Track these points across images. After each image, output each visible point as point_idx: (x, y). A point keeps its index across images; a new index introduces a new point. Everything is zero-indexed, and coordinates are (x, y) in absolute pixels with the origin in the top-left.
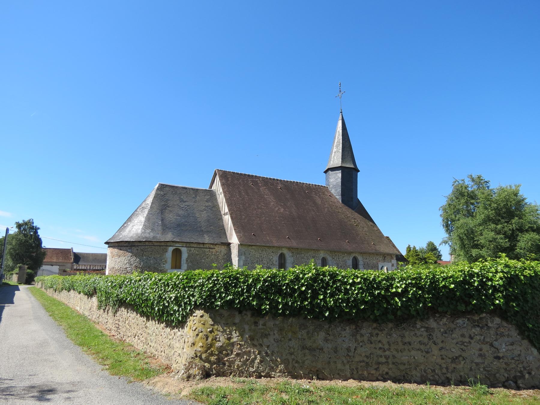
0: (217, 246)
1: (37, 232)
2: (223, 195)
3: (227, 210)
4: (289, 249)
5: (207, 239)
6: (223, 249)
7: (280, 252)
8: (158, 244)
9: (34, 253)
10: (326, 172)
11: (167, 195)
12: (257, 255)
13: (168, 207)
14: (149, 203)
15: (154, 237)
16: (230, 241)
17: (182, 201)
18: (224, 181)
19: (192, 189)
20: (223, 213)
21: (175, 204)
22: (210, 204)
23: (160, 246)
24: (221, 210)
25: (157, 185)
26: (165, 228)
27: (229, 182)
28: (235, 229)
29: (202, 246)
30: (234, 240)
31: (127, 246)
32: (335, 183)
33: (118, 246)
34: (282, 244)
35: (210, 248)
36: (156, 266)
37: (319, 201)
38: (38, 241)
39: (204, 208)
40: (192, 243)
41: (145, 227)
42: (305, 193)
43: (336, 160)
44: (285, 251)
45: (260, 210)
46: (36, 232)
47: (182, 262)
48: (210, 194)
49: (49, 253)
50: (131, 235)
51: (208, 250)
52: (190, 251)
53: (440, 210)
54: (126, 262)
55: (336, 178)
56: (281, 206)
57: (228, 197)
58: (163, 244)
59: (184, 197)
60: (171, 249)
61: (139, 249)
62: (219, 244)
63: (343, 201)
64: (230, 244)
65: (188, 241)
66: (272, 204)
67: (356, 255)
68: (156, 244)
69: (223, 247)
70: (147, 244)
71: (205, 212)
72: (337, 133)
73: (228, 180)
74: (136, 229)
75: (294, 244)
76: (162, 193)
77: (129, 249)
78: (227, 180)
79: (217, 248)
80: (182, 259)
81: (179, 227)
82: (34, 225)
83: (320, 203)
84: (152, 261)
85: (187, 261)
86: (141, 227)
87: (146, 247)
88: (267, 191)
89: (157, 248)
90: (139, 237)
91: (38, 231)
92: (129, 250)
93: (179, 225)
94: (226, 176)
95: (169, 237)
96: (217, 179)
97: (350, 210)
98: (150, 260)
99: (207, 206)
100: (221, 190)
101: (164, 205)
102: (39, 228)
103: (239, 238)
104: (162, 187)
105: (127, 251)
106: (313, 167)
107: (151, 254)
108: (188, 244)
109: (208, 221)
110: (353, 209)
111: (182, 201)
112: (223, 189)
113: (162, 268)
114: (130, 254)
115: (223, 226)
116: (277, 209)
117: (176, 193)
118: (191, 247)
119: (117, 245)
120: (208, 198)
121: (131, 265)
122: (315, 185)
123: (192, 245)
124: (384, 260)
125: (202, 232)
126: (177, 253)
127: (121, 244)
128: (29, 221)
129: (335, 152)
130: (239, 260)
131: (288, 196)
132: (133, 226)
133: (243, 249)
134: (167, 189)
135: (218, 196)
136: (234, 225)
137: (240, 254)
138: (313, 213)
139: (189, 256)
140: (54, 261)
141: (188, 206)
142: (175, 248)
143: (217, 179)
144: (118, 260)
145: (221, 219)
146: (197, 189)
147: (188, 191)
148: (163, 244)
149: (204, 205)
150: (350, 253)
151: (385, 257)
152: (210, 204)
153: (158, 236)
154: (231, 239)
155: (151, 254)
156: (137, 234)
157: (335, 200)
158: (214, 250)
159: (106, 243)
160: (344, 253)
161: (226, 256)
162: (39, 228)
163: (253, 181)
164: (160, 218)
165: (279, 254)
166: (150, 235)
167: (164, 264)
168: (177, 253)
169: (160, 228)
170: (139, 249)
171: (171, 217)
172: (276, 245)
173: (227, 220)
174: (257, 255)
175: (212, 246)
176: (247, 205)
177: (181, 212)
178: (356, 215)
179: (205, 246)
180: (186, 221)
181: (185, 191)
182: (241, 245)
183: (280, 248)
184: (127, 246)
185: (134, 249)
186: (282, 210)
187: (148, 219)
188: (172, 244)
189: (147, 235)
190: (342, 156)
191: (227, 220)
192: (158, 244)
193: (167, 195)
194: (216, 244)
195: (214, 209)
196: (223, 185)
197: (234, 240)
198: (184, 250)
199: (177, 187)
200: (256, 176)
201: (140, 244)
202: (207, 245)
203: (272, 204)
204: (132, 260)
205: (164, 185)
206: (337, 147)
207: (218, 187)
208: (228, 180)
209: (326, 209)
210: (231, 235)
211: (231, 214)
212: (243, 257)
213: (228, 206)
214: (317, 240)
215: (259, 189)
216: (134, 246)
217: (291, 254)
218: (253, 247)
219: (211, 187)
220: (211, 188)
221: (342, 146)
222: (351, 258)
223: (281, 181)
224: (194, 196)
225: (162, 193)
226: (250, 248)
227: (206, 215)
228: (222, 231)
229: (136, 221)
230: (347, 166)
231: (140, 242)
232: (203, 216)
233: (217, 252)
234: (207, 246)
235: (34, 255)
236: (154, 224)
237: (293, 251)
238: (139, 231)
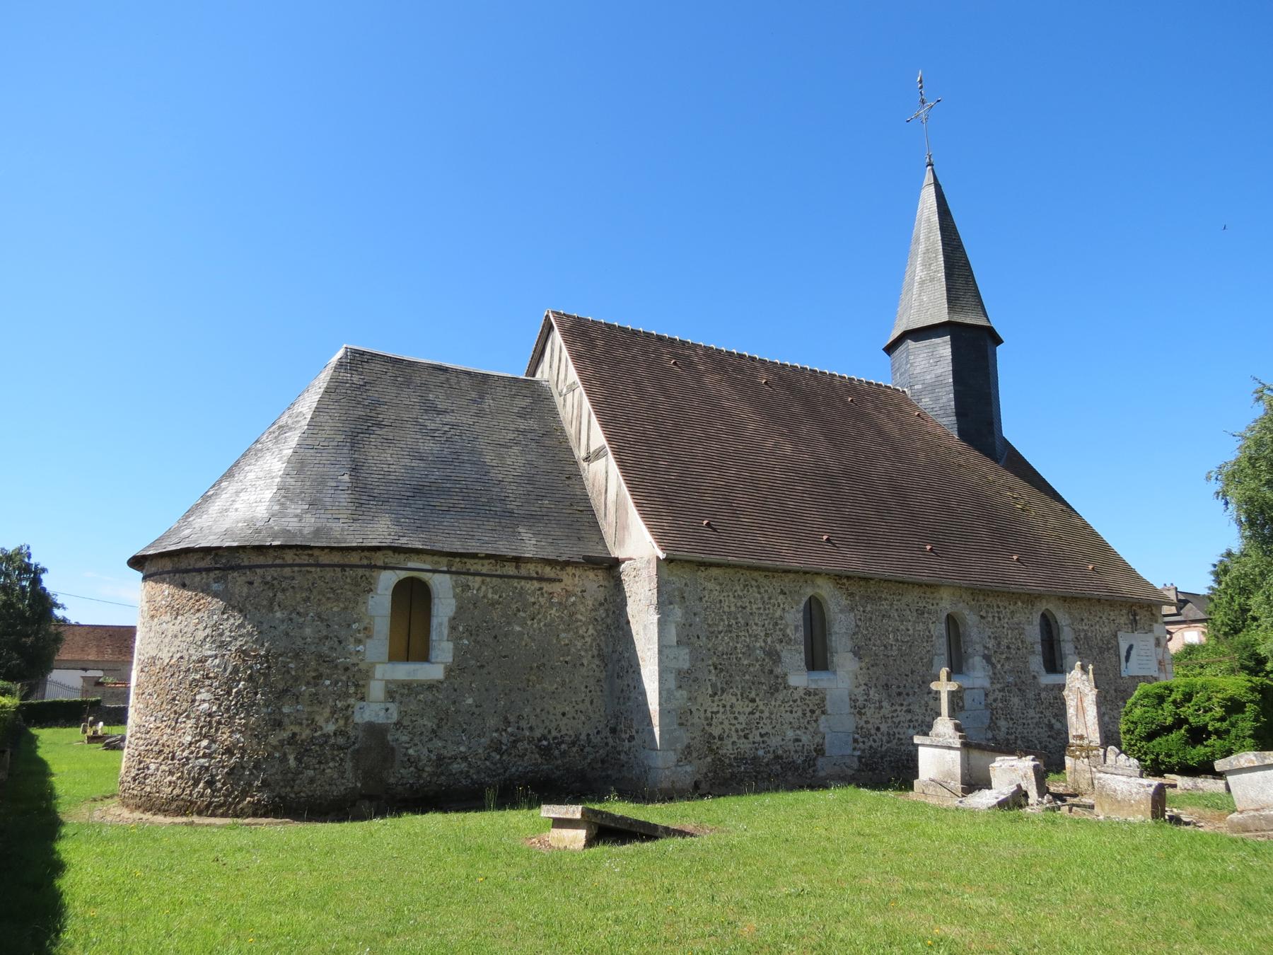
0: (570, 570)
1: (40, 581)
2: (580, 389)
3: (598, 438)
4: (839, 578)
5: (529, 544)
6: (592, 582)
7: (809, 591)
8: (336, 558)
9: (28, 636)
10: (890, 349)
11: (371, 389)
12: (730, 604)
13: (379, 425)
14: (305, 410)
15: (317, 532)
16: (616, 553)
17: (431, 409)
18: (579, 346)
19: (468, 373)
20: (581, 453)
21: (405, 416)
22: (533, 424)
23: (343, 567)
24: (573, 444)
25: (340, 353)
26: (365, 496)
27: (597, 352)
28: (637, 505)
29: (510, 569)
30: (637, 544)
31: (208, 570)
32: (929, 378)
33: (176, 571)
34: (812, 563)
35: (541, 579)
36: (325, 650)
37: (891, 427)
38: (43, 603)
39: (511, 436)
40: (474, 556)
41: (285, 494)
42: (845, 403)
43: (926, 300)
44: (825, 589)
45: (715, 445)
46: (36, 581)
47: (434, 636)
48: (533, 397)
49: (68, 637)
50: (227, 524)
51: (536, 585)
52: (467, 587)
53: (1208, 478)
54: (201, 635)
55: (932, 365)
56: (782, 434)
57: (599, 397)
58: (354, 559)
59: (438, 398)
60: (387, 581)
61: (257, 581)
62: (575, 564)
63: (963, 434)
64: (617, 562)
65: (457, 547)
66: (751, 426)
67: (1051, 607)
68: (325, 558)
69: (591, 574)
70: (289, 557)
71: (516, 449)
72: (924, 225)
73: (595, 347)
74: (250, 504)
75: (853, 562)
76: (356, 378)
77: (217, 580)
78: (591, 344)
79: (572, 580)
80: (435, 622)
81: (420, 496)
82: (32, 561)
83: (896, 433)
84: (308, 631)
85: (453, 628)
86: (268, 495)
87: (287, 571)
88: (726, 390)
89: (329, 574)
90: (258, 531)
91: (43, 576)
92: (215, 586)
93: (419, 491)
94: (585, 333)
95: (380, 531)
96: (557, 337)
97: (989, 462)
98: (301, 626)
99: (523, 432)
100: (573, 376)
101: (366, 419)
102: (44, 570)
103: (661, 537)
104: (357, 360)
105: (206, 590)
106: (857, 321)
107: (307, 599)
108: (457, 561)
109: (531, 480)
110: (997, 461)
111: (431, 409)
112: (580, 372)
113: (354, 660)
114: (218, 604)
115: (586, 499)
116: (770, 444)
117: (408, 383)
118: (468, 573)
119: (168, 564)
120: (524, 404)
121: (222, 645)
122: (869, 384)
123: (473, 566)
124: (1134, 624)
125: (509, 519)
126: (413, 597)
127: (184, 563)
128: (19, 552)
129: (922, 283)
130: (661, 623)
131: (796, 409)
132: (237, 493)
133: (680, 577)
134: (377, 367)
135: (559, 401)
136: (633, 489)
137: (665, 601)
138: (887, 464)
139: (460, 609)
140: (90, 658)
141: (453, 426)
142: (403, 575)
143: (557, 337)
144: (172, 629)
145: (575, 475)
146: (486, 377)
147: (453, 381)
148: (354, 559)
149: (512, 427)
150: (1031, 598)
151: (1135, 615)
152: (533, 424)
153: (337, 526)
154: (620, 542)
155: (307, 599)
156: (250, 522)
157: (939, 431)
158: (557, 588)
159: (137, 562)
160: (1014, 596)
161: (602, 612)
162: (44, 570)
163: (675, 356)
164: (346, 462)
165: (805, 599)
166: (300, 523)
167: (359, 642)
168: (413, 597)
169: (344, 498)
170: (257, 581)
171: (389, 460)
172: (794, 565)
173: (605, 478)
174: (730, 604)
175: (548, 571)
176: (669, 424)
177: (428, 446)
178: (1010, 478)
179: (523, 572)
180: (447, 479)
181: (443, 377)
182: (667, 564)
183: (808, 574)
184: (208, 570)
185: (237, 582)
186: (788, 449)
187: (298, 465)
188: (392, 559)
189: (293, 524)
190: (948, 290)
191: (605, 478)
192: (336, 558)
193: (371, 389)
194: (567, 563)
195: (548, 442)
196: (577, 357)
197: (637, 544)
198: (442, 586)
199: (411, 364)
200: (683, 343)
201: (261, 560)
202: (531, 567)
203: (751, 426)
204: (226, 625)
205: (363, 353)
206: (927, 265)
207: (561, 371)
208: (595, 347)
209: (921, 455)
210: (621, 526)
211: (617, 453)
212: (677, 612)
213: (604, 425)
214: (923, 550)
215: (699, 381)
216: (238, 568)
217: (845, 602)
218: (715, 572)
219: (533, 370)
220: (534, 375)
221: (945, 262)
222: (1037, 619)
223: (763, 362)
224: (474, 395)
225: (356, 378)
226: (702, 574)
227: (521, 461)
228: (582, 516)
229: (251, 476)
230: (969, 321)
231: (260, 549)
232: (510, 464)
233: (569, 594)
234: (531, 569)
235: (29, 641)
236: (321, 481)
237: (853, 589)
238: (261, 511)
